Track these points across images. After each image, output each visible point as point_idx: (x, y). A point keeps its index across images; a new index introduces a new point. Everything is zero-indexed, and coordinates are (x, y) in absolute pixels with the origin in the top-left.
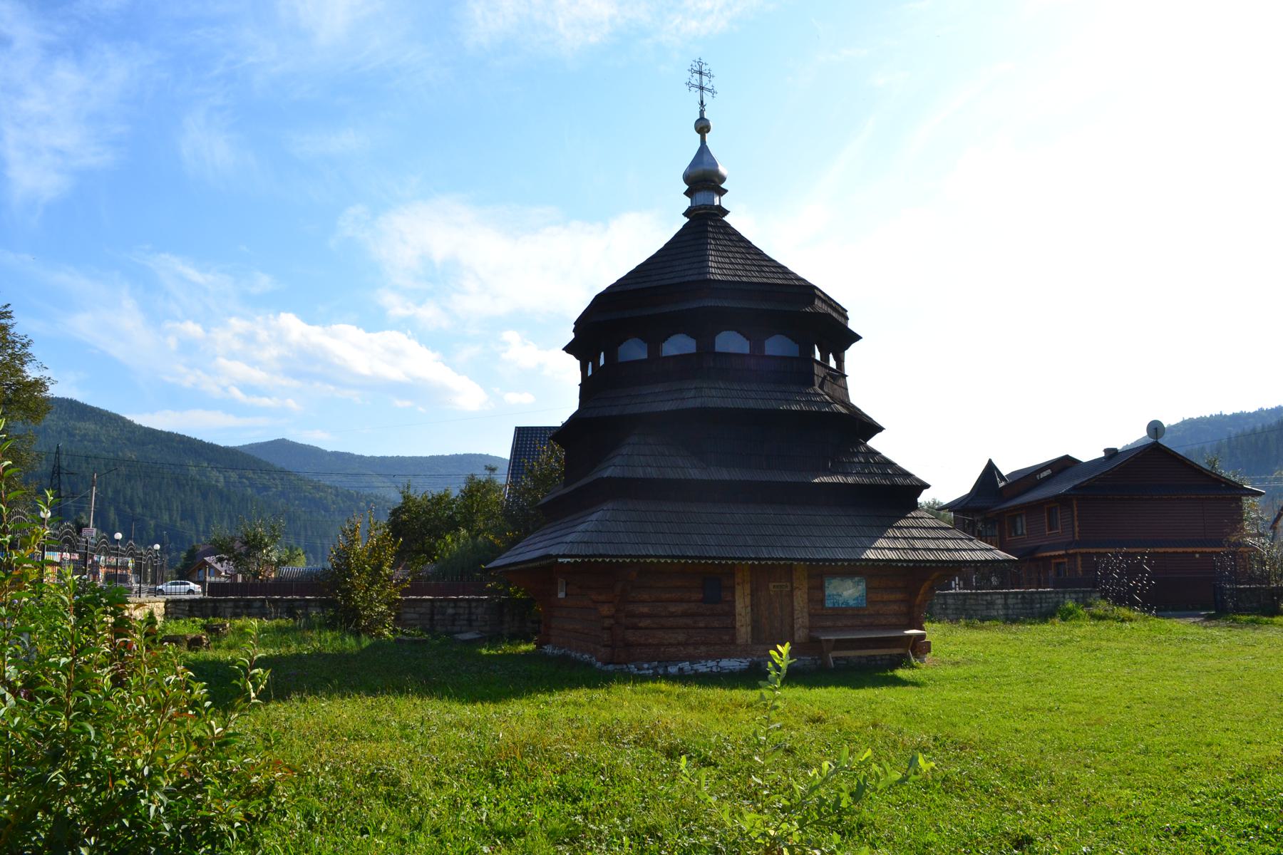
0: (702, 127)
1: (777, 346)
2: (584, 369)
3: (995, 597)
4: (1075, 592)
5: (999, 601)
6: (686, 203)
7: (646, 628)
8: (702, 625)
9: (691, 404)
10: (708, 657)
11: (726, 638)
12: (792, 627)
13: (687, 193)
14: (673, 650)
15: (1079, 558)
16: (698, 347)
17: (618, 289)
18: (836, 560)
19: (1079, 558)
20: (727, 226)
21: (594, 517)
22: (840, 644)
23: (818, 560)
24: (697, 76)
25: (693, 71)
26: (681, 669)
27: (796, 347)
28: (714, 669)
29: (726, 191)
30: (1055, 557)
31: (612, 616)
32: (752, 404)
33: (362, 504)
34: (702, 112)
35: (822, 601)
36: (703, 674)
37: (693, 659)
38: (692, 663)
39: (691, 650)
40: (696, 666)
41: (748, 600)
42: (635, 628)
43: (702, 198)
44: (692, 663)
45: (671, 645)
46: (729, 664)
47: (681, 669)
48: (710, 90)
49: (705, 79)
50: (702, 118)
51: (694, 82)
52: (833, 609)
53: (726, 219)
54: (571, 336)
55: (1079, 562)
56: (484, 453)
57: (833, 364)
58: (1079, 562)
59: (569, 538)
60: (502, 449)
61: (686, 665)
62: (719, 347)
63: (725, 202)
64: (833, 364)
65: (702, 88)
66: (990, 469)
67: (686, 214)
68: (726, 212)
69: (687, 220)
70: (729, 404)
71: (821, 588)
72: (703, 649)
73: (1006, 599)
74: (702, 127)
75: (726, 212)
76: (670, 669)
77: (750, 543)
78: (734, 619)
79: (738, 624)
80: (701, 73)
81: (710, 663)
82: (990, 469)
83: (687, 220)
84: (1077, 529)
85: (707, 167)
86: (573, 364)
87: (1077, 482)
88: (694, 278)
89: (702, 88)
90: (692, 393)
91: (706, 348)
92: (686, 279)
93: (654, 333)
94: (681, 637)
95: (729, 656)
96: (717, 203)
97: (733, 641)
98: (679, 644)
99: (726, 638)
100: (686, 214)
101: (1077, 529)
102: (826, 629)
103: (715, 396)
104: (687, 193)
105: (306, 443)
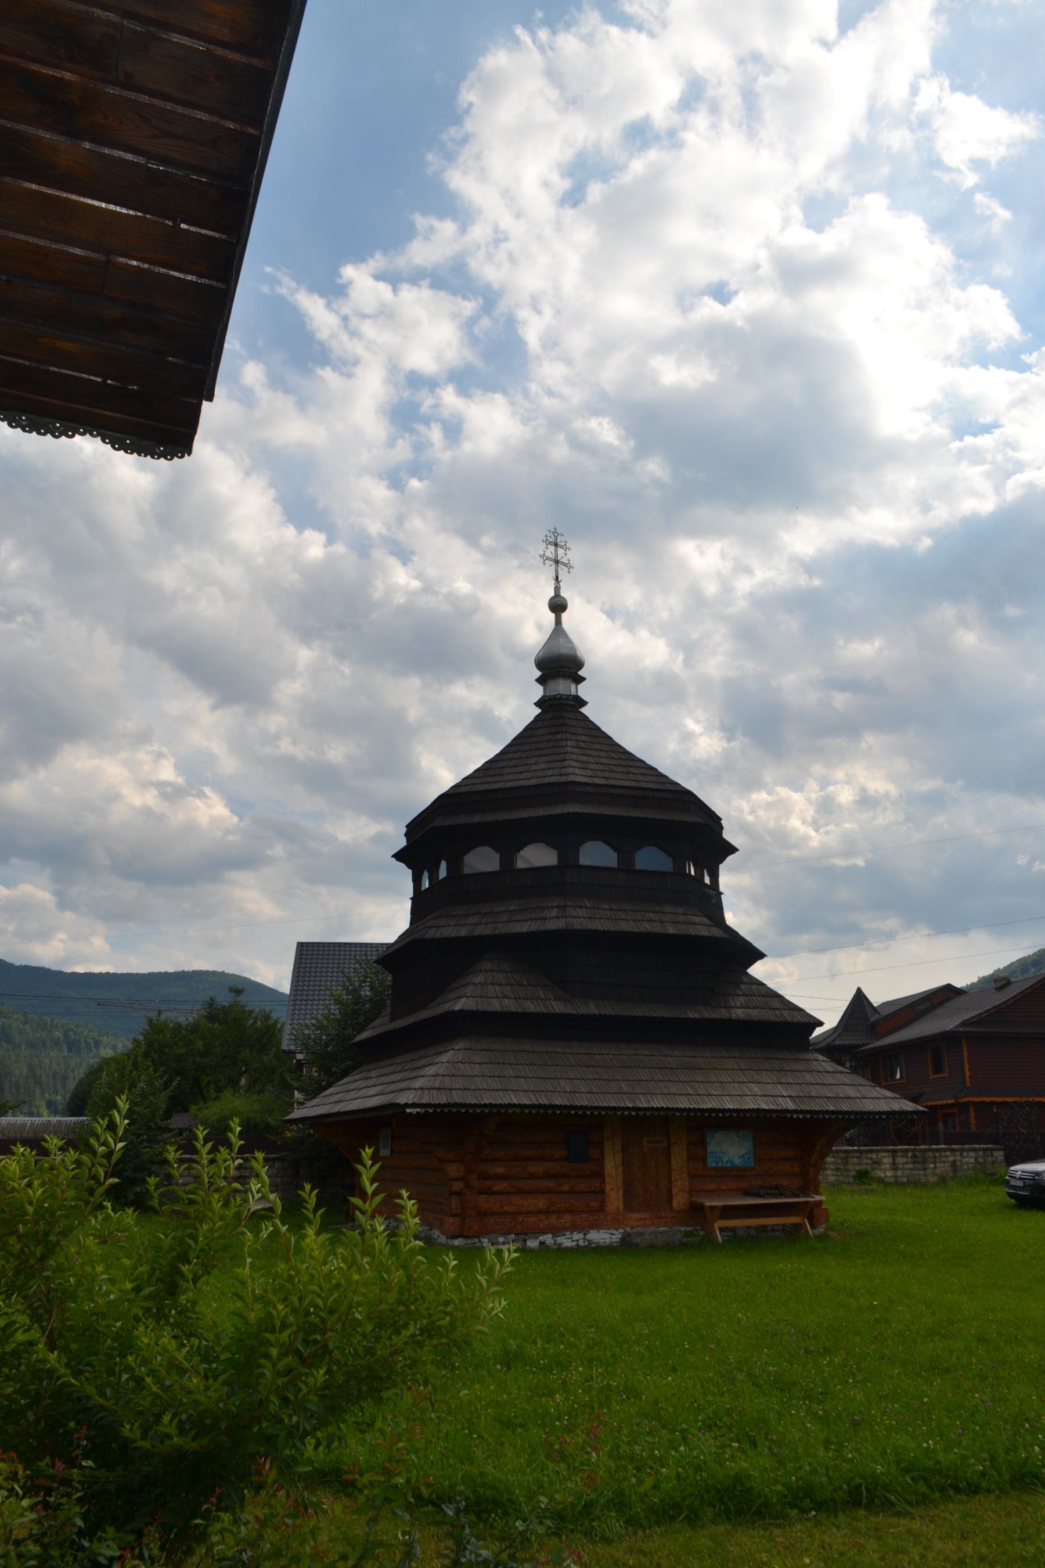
0: (558, 606)
1: (650, 859)
2: (417, 880)
3: (881, 1155)
4: (974, 1150)
5: (885, 1160)
6: (538, 692)
7: (501, 1193)
8: (566, 1188)
9: (552, 925)
10: (574, 1228)
11: (595, 1204)
12: (670, 1191)
13: (538, 680)
14: (532, 1219)
15: (972, 1109)
16: (560, 858)
17: (462, 790)
18: (724, 1111)
19: (972, 1109)
20: (586, 719)
21: (445, 1058)
22: (729, 1212)
23: (703, 1110)
24: (552, 548)
25: (547, 543)
26: (542, 1243)
27: (615, 855)
28: (581, 1243)
29: (583, 679)
30: (942, 1107)
31: (461, 1179)
32: (623, 927)
33: (58, 1034)
34: (557, 589)
35: (704, 1159)
36: (568, 1250)
37: (556, 1231)
38: (555, 1236)
39: (553, 1219)
40: (560, 1240)
41: (619, 1157)
42: (489, 1192)
43: (562, 687)
44: (555, 1236)
45: (530, 1213)
46: (600, 1236)
47: (542, 1243)
48: (565, 565)
49: (561, 551)
50: (557, 594)
51: (548, 554)
52: (716, 1169)
53: (583, 710)
54: (403, 842)
55: (972, 1114)
56: (163, 971)
57: (707, 880)
58: (972, 1114)
59: (418, 1084)
60: (276, 974)
61: (548, 1239)
62: (584, 861)
63: (583, 691)
64: (707, 880)
65: (557, 562)
66: (860, 998)
67: (538, 704)
68: (584, 703)
69: (538, 711)
70: (598, 925)
71: (703, 1144)
72: (567, 1218)
73: (894, 1157)
74: (558, 606)
75: (584, 703)
76: (529, 1243)
77: (625, 1090)
78: (604, 1182)
79: (608, 1188)
80: (556, 545)
81: (577, 1236)
82: (860, 998)
83: (538, 711)
84: (968, 1073)
85: (563, 651)
86: (404, 876)
87: (966, 1016)
88: (553, 780)
89: (557, 562)
90: (554, 913)
91: (568, 861)
92: (546, 780)
93: (508, 839)
94: (542, 1203)
95: (597, 1226)
96: (573, 692)
97: (602, 1208)
98: (540, 1212)
99: (595, 1204)
100: (538, 704)
101: (968, 1073)
102: (709, 1193)
103: (583, 917)
104: (538, 680)
105: (259, 980)
